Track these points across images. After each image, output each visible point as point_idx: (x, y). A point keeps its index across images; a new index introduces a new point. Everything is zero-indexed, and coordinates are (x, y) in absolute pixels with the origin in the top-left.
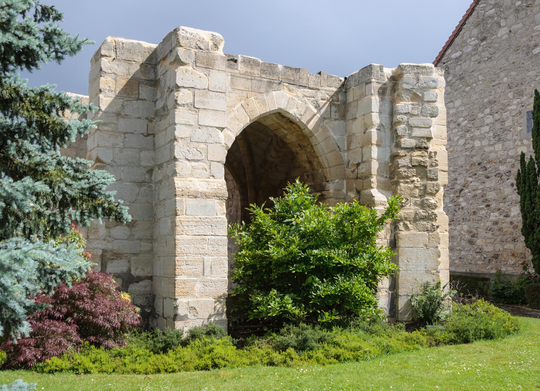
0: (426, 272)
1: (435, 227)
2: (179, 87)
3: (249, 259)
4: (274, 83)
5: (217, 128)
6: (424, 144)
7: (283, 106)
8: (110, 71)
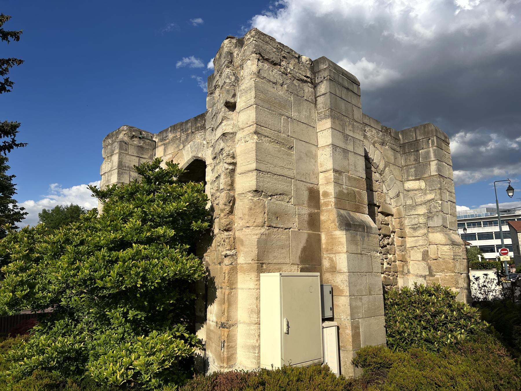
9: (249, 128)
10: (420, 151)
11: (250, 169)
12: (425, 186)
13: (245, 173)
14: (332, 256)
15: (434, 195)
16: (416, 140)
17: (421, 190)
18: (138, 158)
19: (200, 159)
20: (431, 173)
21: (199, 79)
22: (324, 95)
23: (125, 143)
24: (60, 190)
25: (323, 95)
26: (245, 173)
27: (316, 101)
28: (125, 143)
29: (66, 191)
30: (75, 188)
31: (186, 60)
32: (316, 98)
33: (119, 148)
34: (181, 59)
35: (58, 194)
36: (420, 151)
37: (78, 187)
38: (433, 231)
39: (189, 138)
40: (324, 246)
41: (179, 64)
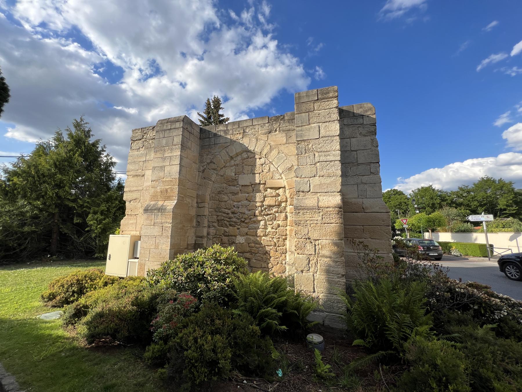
13: (245, 186)
21: (502, 69)
23: (366, 136)
24: (403, 180)
28: (366, 136)
29: (407, 180)
30: (412, 178)
31: (487, 61)
33: (181, 149)
34: (479, 63)
35: (403, 183)
37: (414, 177)
41: (479, 68)
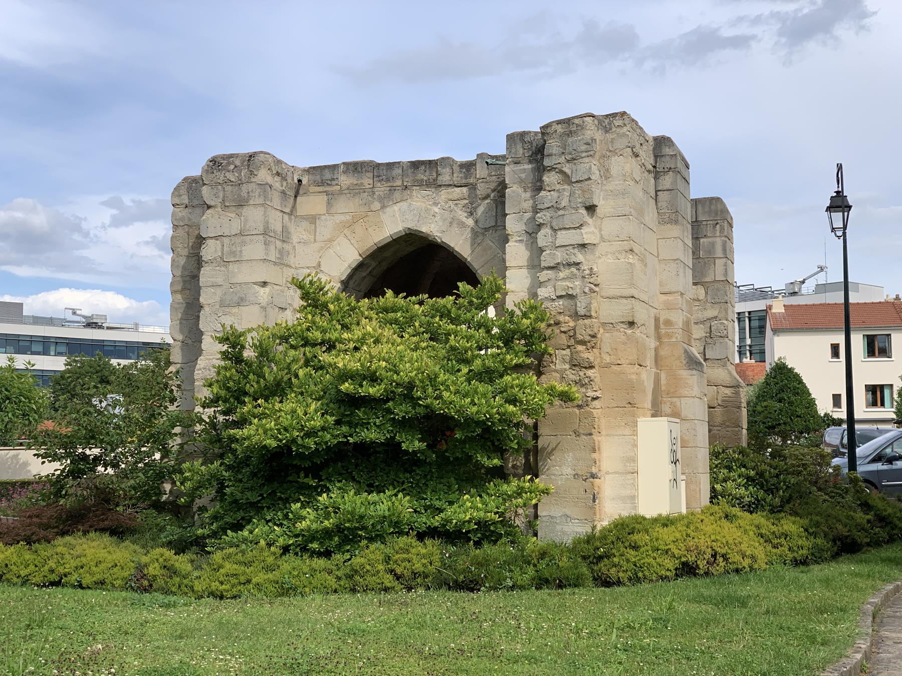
0: (574, 476)
1: (590, 399)
2: (204, 239)
3: (70, 520)
4: (395, 190)
5: (255, 283)
6: (573, 256)
7: (412, 225)
8: (182, 224)
9: (621, 242)
10: (702, 240)
11: (623, 295)
12: (704, 295)
14: (675, 400)
15: (718, 310)
16: (696, 221)
17: (698, 300)
18: (281, 214)
19: (421, 235)
20: (715, 276)
22: (669, 192)
25: (667, 190)
26: (613, 298)
27: (656, 195)
32: (656, 191)
36: (702, 240)
38: (713, 365)
39: (397, 195)
40: (663, 388)
